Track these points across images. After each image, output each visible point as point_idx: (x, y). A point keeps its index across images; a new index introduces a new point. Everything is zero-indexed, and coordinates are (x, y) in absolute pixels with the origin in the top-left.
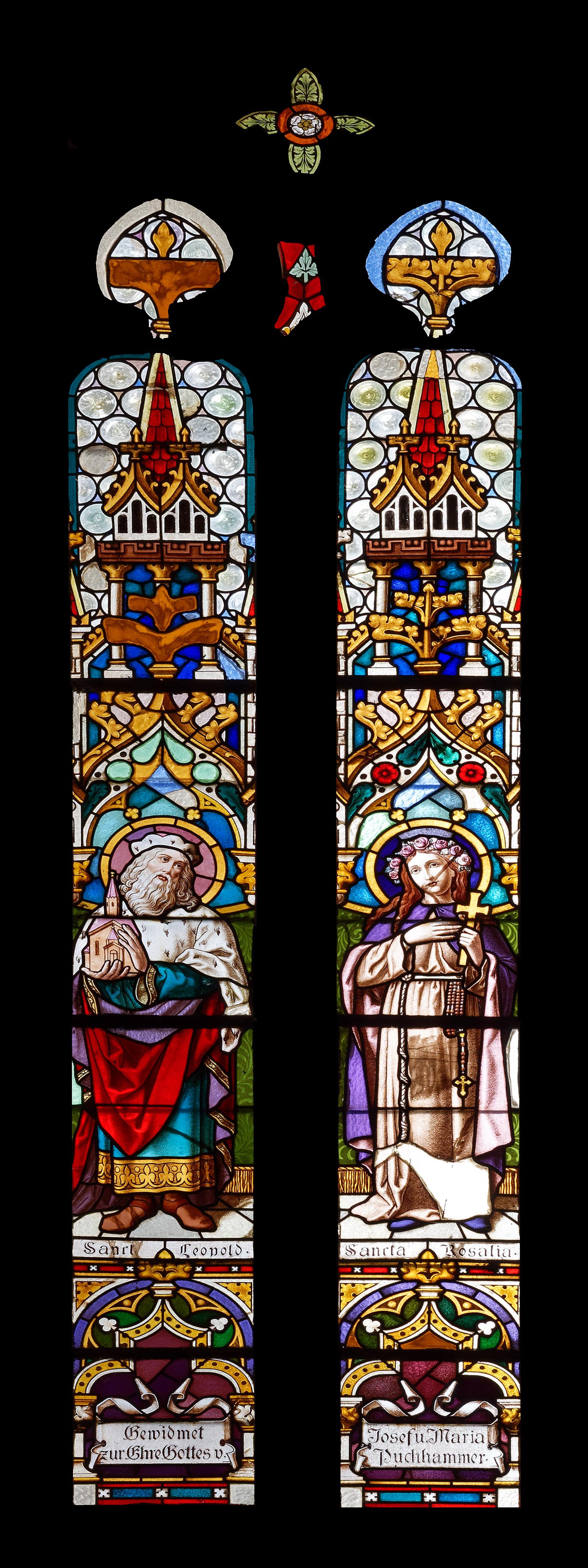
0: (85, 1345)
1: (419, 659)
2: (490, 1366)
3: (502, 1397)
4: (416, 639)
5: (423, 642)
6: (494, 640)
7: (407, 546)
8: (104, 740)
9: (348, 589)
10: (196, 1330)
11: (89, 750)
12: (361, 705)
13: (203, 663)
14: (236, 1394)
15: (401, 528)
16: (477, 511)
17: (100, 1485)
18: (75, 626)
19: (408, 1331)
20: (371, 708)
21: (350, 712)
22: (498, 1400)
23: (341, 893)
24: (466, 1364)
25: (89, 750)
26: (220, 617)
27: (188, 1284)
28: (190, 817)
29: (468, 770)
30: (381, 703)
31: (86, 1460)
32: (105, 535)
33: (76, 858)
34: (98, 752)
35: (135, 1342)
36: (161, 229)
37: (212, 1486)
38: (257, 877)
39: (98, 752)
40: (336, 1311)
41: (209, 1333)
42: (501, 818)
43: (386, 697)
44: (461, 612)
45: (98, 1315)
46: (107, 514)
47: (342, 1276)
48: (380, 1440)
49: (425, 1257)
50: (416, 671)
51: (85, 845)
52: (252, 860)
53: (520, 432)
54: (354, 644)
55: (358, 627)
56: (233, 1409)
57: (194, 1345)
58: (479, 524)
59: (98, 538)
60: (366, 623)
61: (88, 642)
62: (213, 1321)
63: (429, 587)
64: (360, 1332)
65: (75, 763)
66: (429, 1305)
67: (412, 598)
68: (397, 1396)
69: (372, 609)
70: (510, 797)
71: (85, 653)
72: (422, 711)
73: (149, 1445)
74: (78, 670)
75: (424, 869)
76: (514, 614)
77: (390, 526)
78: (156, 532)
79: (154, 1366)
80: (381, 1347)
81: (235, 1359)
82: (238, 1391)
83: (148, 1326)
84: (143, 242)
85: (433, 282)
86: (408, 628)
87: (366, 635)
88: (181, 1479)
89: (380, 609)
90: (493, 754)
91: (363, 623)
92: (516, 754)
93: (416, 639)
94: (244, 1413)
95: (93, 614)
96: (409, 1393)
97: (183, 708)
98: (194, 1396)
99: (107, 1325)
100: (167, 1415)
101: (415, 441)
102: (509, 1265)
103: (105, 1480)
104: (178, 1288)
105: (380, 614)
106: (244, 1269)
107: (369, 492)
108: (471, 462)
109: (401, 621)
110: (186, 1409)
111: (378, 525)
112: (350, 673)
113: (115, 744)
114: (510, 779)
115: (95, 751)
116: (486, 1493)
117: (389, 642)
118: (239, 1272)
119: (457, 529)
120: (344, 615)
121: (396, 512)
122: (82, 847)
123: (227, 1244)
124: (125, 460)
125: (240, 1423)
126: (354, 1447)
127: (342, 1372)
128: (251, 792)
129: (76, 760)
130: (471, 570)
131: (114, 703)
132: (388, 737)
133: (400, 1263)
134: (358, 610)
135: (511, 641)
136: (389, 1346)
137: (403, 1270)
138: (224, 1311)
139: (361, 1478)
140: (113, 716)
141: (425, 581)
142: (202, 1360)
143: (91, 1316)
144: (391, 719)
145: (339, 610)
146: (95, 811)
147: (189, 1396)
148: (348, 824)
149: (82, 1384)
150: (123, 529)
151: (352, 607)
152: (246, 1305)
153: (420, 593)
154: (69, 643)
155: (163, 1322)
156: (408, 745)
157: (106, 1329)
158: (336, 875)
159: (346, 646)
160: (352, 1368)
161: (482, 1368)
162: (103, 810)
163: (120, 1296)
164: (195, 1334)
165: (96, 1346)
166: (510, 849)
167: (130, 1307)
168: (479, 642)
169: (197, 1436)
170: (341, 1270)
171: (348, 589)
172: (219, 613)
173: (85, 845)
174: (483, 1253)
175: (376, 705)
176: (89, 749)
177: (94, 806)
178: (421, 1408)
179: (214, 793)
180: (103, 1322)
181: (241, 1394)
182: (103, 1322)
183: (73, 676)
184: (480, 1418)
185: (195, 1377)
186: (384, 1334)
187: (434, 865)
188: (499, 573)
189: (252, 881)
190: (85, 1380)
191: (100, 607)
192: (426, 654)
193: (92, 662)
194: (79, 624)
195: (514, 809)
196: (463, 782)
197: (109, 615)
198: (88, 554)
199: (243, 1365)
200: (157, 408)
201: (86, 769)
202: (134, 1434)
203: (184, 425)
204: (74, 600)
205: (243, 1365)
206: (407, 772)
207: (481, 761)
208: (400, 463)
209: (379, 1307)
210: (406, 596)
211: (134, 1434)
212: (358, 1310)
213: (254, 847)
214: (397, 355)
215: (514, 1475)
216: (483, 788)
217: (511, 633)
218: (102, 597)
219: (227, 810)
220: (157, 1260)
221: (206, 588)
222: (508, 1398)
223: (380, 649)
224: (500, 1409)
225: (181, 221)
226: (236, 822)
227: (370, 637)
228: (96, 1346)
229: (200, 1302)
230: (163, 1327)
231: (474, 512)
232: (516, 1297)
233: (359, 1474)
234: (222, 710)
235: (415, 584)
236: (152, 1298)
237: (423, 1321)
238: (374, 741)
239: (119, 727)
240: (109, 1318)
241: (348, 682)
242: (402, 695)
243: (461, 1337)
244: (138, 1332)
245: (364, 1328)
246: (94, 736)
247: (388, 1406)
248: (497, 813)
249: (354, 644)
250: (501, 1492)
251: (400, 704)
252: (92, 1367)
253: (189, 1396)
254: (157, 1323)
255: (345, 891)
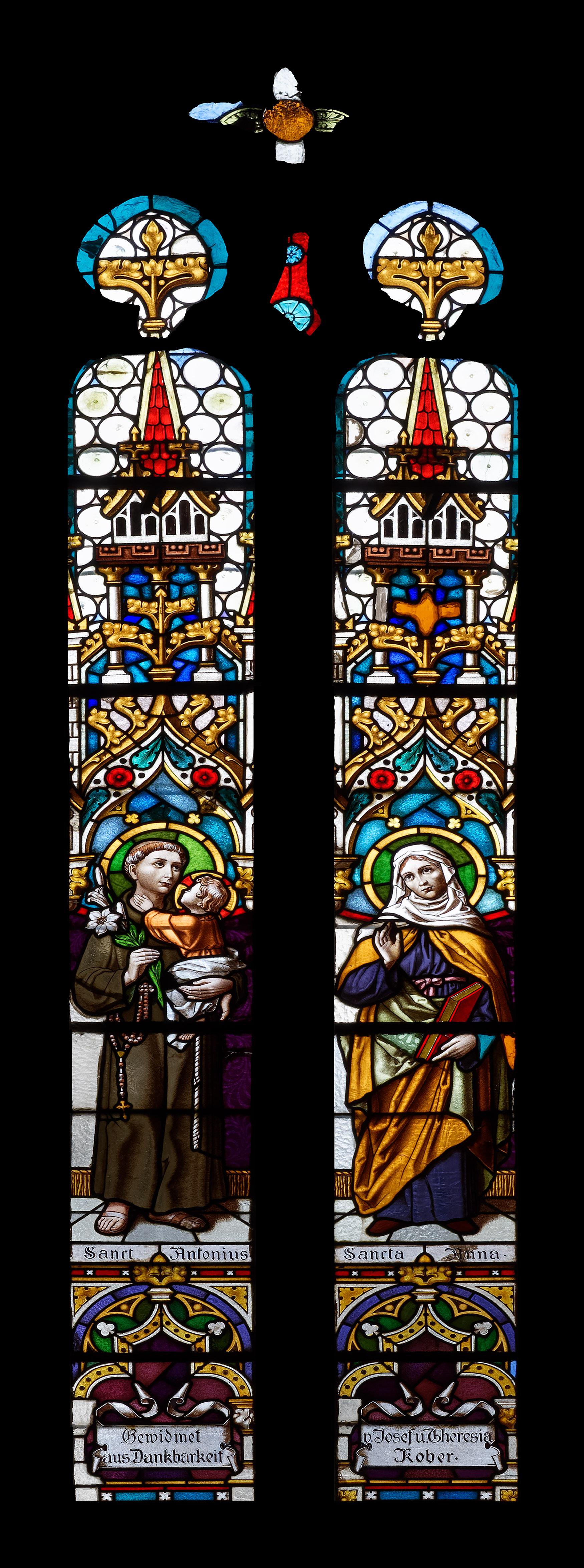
0: (350, 1348)
1: (154, 665)
2: (486, 1367)
3: (499, 1397)
4: (151, 646)
5: (158, 649)
6: (491, 650)
7: (137, 551)
8: (367, 748)
9: (80, 597)
10: (460, 1335)
11: (88, 757)
12: (94, 711)
13: (465, 669)
14: (501, 1397)
15: (182, 533)
16: (475, 522)
17: (367, 1487)
18: (71, 632)
19: (407, 1334)
20: (367, 714)
21: (83, 719)
22: (496, 1400)
23: (338, 900)
24: (198, 1365)
25: (88, 757)
26: (484, 624)
27: (183, 1288)
28: (451, 826)
29: (379, 777)
30: (114, 709)
31: (352, 1462)
32: (104, 538)
33: (73, 865)
34: (97, 760)
35: (399, 1347)
36: (427, 230)
37: (214, 1490)
38: (516, 883)
39: (97, 760)
40: (69, 1315)
41: (473, 1337)
42: (495, 826)
43: (119, 703)
44: (193, 617)
45: (97, 1319)
46: (106, 517)
47: (74, 1279)
48: (188, 1441)
49: (423, 1260)
50: (414, 679)
51: (84, 851)
52: (511, 866)
53: (516, 441)
54: (88, 653)
55: (91, 635)
56: (232, 1412)
57: (458, 1350)
58: (212, 529)
59: (97, 542)
60: (100, 630)
61: (86, 648)
62: (477, 1326)
63: (161, 593)
64: (360, 1337)
65: (74, 771)
66: (161, 1308)
67: (145, 604)
68: (131, 1398)
69: (106, 616)
70: (505, 804)
71: (83, 659)
72: (418, 717)
73: (148, 1449)
74: (76, 677)
75: (417, 875)
76: (509, 625)
77: (122, 532)
78: (421, 537)
79: (152, 1370)
80: (381, 1349)
81: (234, 1364)
82: (237, 1395)
83: (412, 1331)
84: (410, 241)
85: (423, 283)
86: (407, 639)
87: (100, 643)
88: (183, 1482)
89: (114, 616)
90: (489, 760)
91: (96, 631)
92: (511, 761)
93: (151, 646)
94: (244, 1416)
95: (91, 618)
96: (143, 1395)
97: (445, 713)
98: (192, 1399)
99: (370, 1330)
100: (170, 1420)
101: (146, 447)
102: (364, 1268)
103: (372, 1482)
104: (176, 1293)
105: (114, 622)
106: (504, 1273)
107: (99, 499)
108: (202, 468)
109: (134, 629)
110: (451, 1412)
111: (109, 531)
112: (83, 681)
113: (115, 751)
114: (243, 783)
115: (95, 758)
116: (483, 1490)
117: (388, 652)
118: (94, 1276)
119: (140, 535)
120: (76, 623)
121: (395, 520)
122: (81, 854)
123: (219, 1248)
124: (393, 463)
125: (239, 1427)
126: (354, 1447)
127: (340, 1376)
128: (511, 798)
129: (75, 768)
130: (469, 580)
131: (377, 708)
132: (122, 742)
133: (132, 1266)
134: (357, 617)
135: (507, 651)
136: (388, 1350)
137: (401, 1273)
138: (222, 1317)
139: (362, 1477)
140: (113, 723)
141: (157, 587)
142: (466, 1364)
143: (354, 1321)
144: (123, 724)
145: (71, 617)
146: (358, 819)
147: (454, 1400)
148: (82, 829)
149: (82, 1388)
150: (389, 534)
151: (84, 615)
152: (509, 1310)
153: (153, 598)
154: (65, 649)
155: (426, 1326)
156: (405, 751)
157: (368, 1334)
158: (333, 882)
159: (346, 654)
160: (85, 1371)
161: (479, 1368)
162: (101, 818)
163: (382, 1301)
164: (459, 1338)
165: (359, 1349)
166: (505, 856)
167: (393, 1312)
168: (476, 652)
169: (194, 1439)
170: (74, 1273)
171: (80, 597)
172: (481, 619)
173: (84, 851)
174: (363, 1256)
175: (372, 711)
176: (89, 756)
177: (357, 815)
178: (419, 1409)
179: (474, 801)
180: (101, 1326)
181: (240, 1398)
182: (101, 1326)
183: (70, 683)
184: (478, 1418)
185: (460, 1380)
186: (118, 1337)
187: (427, 871)
188: (228, 579)
189: (511, 887)
190: (351, 1384)
191: (98, 611)
192: (159, 661)
193: (355, 667)
194: (77, 629)
195: (509, 816)
196: (457, 789)
197: (108, 620)
198: (85, 556)
199: (241, 1369)
200: (424, 411)
201: (84, 777)
202: (132, 1438)
203: (451, 430)
204: (71, 606)
205: (241, 1369)
206: (404, 779)
207: (476, 768)
208: (132, 469)
209: (111, 1311)
210: (139, 602)
211: (132, 1438)
212: (91, 1314)
213: (252, 851)
214: (122, 361)
215: (248, 1474)
216: (480, 794)
217: (246, 637)
218: (101, 602)
219: (487, 818)
220: (150, 1264)
221: (470, 594)
222: (505, 1397)
223: (114, 657)
224: (497, 1408)
225: (448, 222)
226: (495, 830)
227: (105, 645)
228: (359, 1349)
229: (462, 1307)
230: (427, 1331)
231: (471, 523)
232: (511, 1297)
233: (360, 1473)
234: (483, 714)
235: (147, 591)
236: (414, 1304)
237: (155, 1324)
238: (371, 747)
239: (118, 733)
240: (372, 1324)
241: (84, 690)
242: (135, 701)
243: (193, 1339)
244: (401, 1337)
245: (99, 1332)
246: (93, 742)
247: (121, 1407)
248: (491, 820)
249: (88, 653)
250: (235, 1490)
251: (133, 709)
252: (357, 1372)
253: (454, 1400)
254: (155, 1328)
255: (77, 897)
